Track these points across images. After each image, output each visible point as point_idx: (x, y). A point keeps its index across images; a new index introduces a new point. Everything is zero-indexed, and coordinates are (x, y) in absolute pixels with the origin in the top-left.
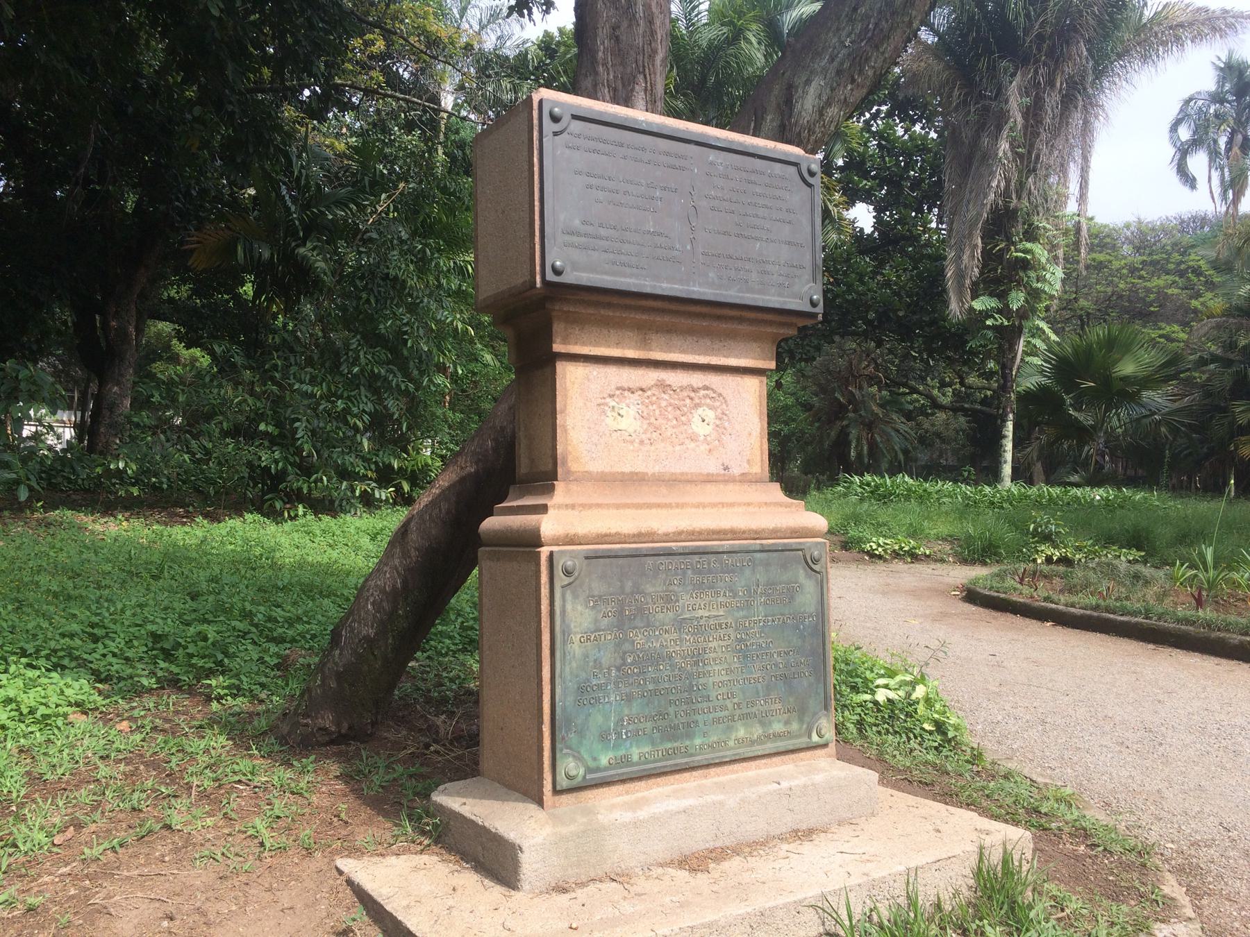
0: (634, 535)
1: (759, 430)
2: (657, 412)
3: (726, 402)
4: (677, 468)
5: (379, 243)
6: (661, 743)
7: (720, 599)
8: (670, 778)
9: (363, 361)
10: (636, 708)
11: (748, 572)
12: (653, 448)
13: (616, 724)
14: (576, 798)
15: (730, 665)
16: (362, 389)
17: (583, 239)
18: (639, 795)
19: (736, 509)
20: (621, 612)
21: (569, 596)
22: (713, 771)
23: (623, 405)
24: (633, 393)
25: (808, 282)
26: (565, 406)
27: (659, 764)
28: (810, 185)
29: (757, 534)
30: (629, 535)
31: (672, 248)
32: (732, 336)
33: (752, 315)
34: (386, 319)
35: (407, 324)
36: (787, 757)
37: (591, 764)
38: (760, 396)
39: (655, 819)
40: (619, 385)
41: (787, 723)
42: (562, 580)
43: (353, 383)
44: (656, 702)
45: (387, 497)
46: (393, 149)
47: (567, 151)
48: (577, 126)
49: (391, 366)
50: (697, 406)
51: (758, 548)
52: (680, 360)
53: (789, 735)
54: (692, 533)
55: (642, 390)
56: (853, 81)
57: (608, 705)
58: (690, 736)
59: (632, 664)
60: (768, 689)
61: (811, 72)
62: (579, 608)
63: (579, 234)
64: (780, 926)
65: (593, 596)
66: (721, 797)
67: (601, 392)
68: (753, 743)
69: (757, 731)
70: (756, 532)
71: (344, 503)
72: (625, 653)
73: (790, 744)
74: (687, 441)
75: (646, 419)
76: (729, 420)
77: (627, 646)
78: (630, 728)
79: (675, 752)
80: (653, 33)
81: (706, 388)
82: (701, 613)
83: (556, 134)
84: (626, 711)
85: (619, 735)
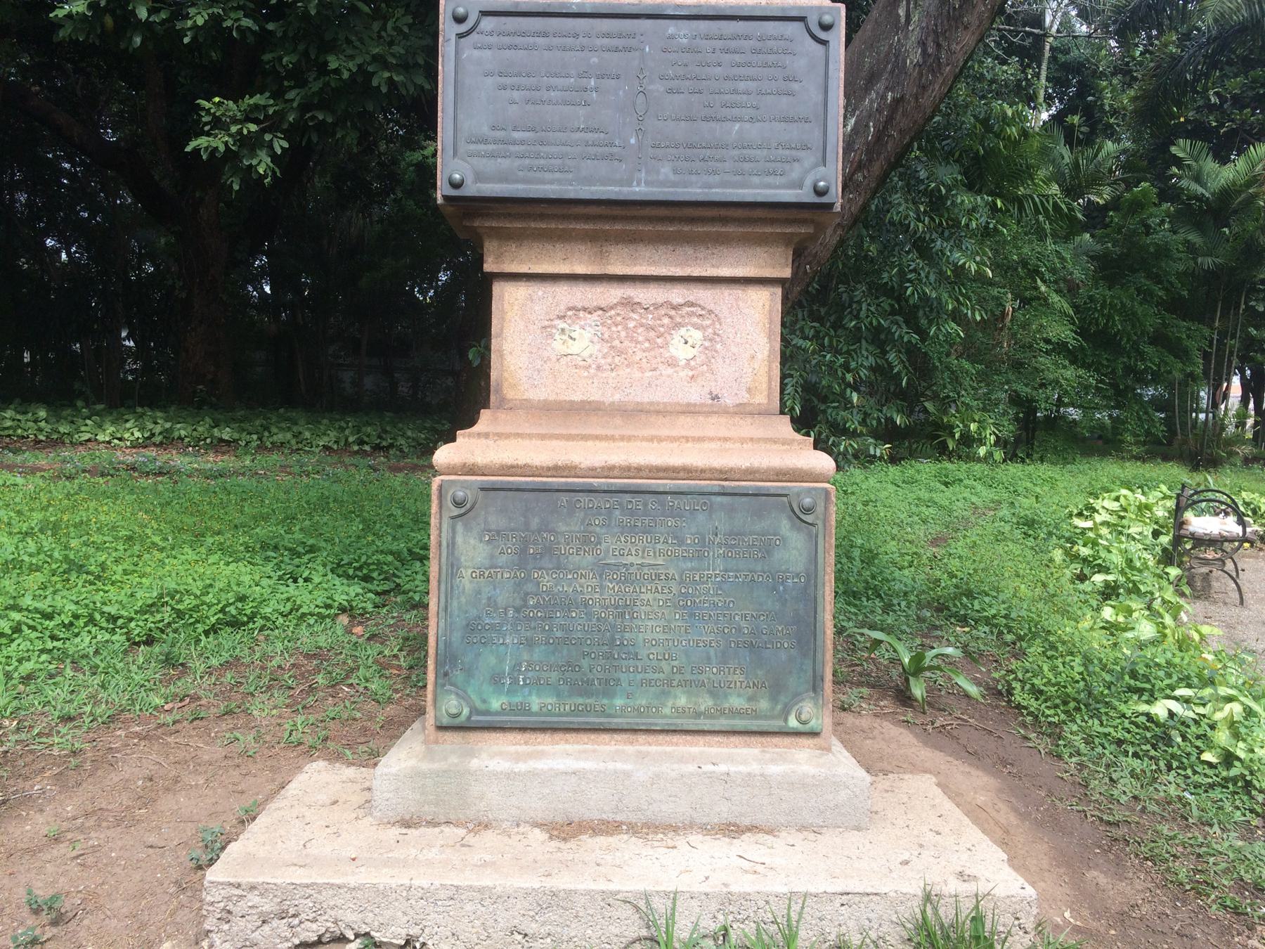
0: (549, 469)
1: (766, 353)
2: (623, 334)
3: (719, 319)
4: (645, 397)
6: (570, 696)
8: (584, 737)
10: (538, 653)
11: (701, 517)
12: (614, 374)
14: (463, 738)
15: (669, 621)
16: (864, 342)
17: (491, 147)
18: (540, 748)
19: (706, 445)
20: (523, 551)
21: (460, 527)
22: (642, 738)
23: (577, 328)
24: (590, 313)
25: (816, 166)
26: (502, 329)
27: (564, 719)
28: (824, 43)
31: (612, 145)
33: (739, 213)
35: (915, 270)
37: (479, 704)
38: (770, 311)
39: (534, 774)
40: (571, 305)
41: (750, 699)
42: (450, 510)
43: (856, 336)
44: (565, 652)
45: (882, 453)
47: (476, 53)
48: (488, 23)
49: (897, 317)
50: (678, 326)
51: (716, 490)
52: (648, 273)
53: (756, 715)
54: (629, 468)
55: (602, 309)
58: (609, 694)
59: (535, 607)
60: (724, 658)
62: (472, 541)
63: (485, 141)
64: (580, 914)
66: (628, 767)
67: (547, 313)
68: (698, 715)
69: (706, 703)
74: (661, 367)
75: (607, 341)
77: (530, 587)
78: (530, 674)
79: (587, 711)
81: (692, 305)
82: (631, 559)
83: (461, 36)
84: (526, 656)
85: (515, 681)
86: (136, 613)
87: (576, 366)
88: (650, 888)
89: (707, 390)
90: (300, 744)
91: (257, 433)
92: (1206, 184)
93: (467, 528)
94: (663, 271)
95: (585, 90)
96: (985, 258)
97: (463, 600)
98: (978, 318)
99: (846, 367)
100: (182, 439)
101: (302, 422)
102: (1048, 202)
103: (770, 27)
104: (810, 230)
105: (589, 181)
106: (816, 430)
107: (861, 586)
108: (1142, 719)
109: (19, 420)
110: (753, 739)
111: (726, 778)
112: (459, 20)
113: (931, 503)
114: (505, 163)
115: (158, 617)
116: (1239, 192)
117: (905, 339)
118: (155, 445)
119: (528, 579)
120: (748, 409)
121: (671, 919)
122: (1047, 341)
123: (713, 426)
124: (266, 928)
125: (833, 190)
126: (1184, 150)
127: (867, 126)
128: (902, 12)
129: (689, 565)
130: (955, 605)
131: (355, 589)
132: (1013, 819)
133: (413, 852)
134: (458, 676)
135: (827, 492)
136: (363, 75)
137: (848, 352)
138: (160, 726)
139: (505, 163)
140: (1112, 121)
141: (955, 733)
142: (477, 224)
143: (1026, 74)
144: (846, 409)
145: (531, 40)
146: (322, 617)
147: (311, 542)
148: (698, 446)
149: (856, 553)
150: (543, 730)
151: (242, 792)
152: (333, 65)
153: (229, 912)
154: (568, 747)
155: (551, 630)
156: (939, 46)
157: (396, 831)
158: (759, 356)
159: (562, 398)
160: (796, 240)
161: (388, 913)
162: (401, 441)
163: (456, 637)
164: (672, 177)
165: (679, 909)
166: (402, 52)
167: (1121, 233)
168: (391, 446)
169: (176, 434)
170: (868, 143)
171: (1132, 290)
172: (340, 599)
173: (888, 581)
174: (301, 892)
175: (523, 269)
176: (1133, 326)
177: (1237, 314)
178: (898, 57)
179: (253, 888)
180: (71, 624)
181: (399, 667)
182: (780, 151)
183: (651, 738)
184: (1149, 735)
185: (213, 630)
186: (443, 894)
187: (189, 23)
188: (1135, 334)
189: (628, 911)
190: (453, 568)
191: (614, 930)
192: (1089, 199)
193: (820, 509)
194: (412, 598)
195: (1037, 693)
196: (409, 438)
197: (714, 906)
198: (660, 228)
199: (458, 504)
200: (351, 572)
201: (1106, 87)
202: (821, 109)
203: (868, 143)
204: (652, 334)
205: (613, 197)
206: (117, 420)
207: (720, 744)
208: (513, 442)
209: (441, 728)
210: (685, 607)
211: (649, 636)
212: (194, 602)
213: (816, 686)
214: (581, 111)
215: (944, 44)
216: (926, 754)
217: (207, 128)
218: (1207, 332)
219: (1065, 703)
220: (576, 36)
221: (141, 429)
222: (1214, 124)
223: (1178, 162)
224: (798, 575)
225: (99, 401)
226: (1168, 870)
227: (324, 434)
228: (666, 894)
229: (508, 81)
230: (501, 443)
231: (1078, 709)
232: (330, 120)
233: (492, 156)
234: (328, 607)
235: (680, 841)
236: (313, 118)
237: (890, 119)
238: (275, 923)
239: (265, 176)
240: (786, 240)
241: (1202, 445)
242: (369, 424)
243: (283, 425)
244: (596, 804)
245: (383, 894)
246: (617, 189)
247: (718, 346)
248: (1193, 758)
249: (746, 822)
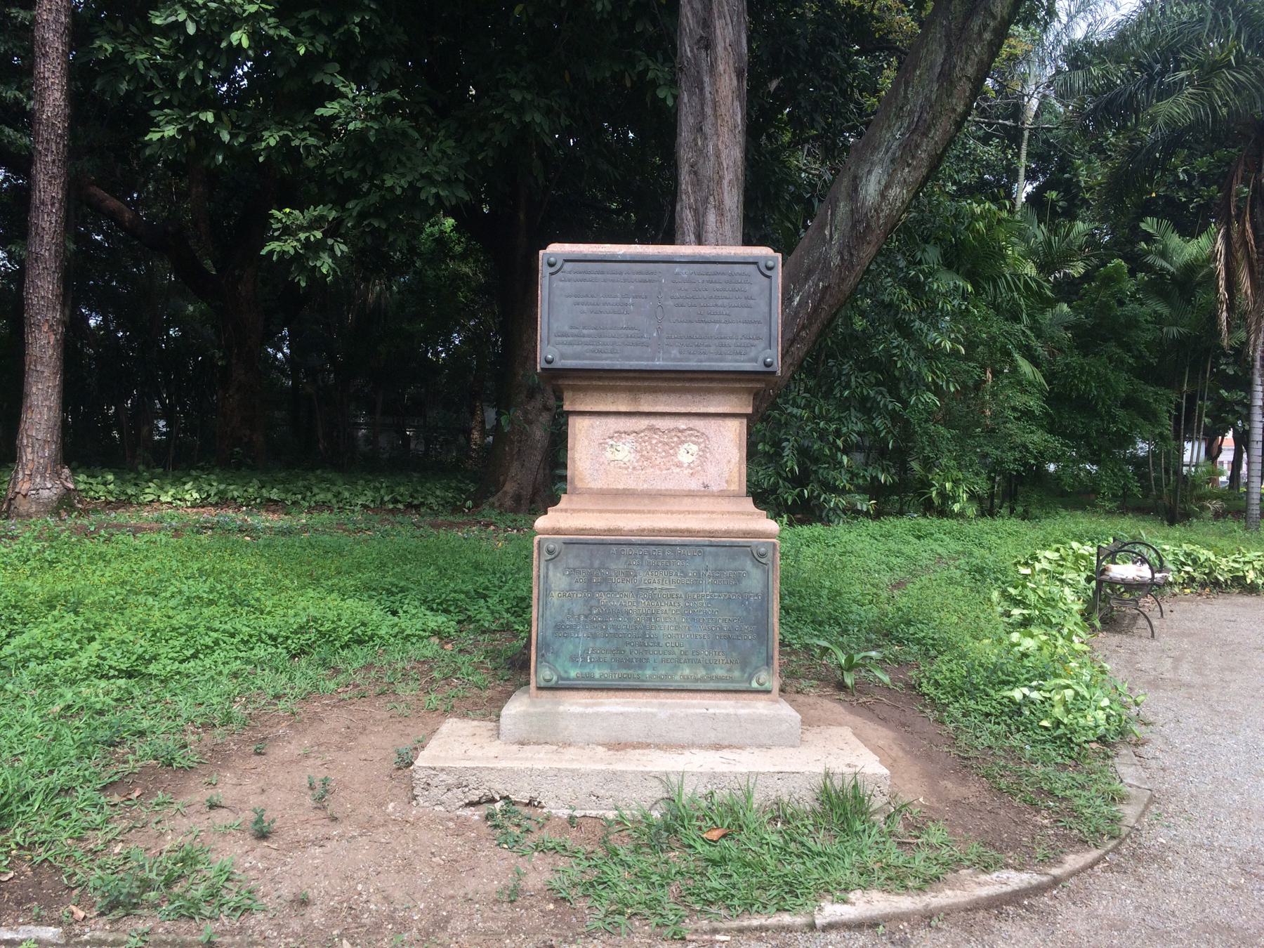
0: (605, 531)
2: (649, 447)
4: (670, 485)
5: (875, 273)
6: (619, 668)
8: (627, 694)
9: (853, 384)
10: (599, 643)
11: (698, 560)
16: (852, 410)
17: (570, 339)
19: (701, 516)
20: (590, 580)
21: (551, 566)
22: (662, 694)
25: (764, 349)
29: (711, 534)
31: (642, 337)
32: (710, 391)
34: (878, 342)
35: (897, 347)
38: (740, 434)
39: (597, 714)
41: (729, 670)
43: (844, 405)
46: (968, 163)
47: (561, 283)
48: (568, 266)
49: (881, 388)
50: (683, 442)
53: (732, 680)
54: (653, 530)
56: (909, 165)
58: (641, 667)
61: (872, 164)
66: (654, 710)
68: (696, 680)
69: (701, 673)
71: (831, 513)
73: (731, 686)
76: (711, 453)
77: (593, 603)
78: (594, 656)
79: (629, 678)
80: (720, 164)
81: (692, 429)
82: (655, 585)
84: (591, 645)
85: (585, 660)
86: (291, 633)
87: (620, 468)
88: (669, 769)
89: (701, 481)
90: (437, 710)
91: (301, 493)
92: (1172, 258)
93: (556, 567)
94: (674, 410)
95: (626, 305)
96: (959, 336)
97: (553, 610)
98: (952, 389)
99: (838, 434)
100: (235, 500)
101: (340, 482)
102: (1019, 280)
103: (737, 268)
104: (763, 385)
105: (628, 358)
106: (809, 488)
107: (824, 617)
108: (1005, 700)
109: (91, 484)
110: (730, 695)
111: (714, 717)
112: (551, 265)
113: (899, 553)
114: (578, 348)
115: (307, 636)
116: (1202, 267)
117: (890, 407)
118: (211, 505)
119: (592, 597)
120: (726, 493)
121: (680, 787)
122: (1014, 409)
123: (705, 504)
124: (449, 793)
125: (775, 363)
126: (1152, 228)
127: (807, 302)
128: (827, 233)
129: (690, 589)
130: (897, 631)
131: (442, 618)
132: (901, 754)
133: (530, 755)
134: (550, 656)
135: (774, 545)
136: (413, 189)
137: (839, 419)
138: (341, 700)
139: (578, 348)
140: (1087, 196)
141: (872, 707)
142: (560, 382)
143: (1006, 154)
144: (835, 469)
145: (594, 276)
146: (421, 638)
147: (402, 584)
148: (695, 516)
149: (825, 592)
150: (601, 689)
151: (409, 735)
152: (389, 183)
153: (429, 784)
154: (617, 700)
155: (606, 628)
156: (852, 255)
157: (516, 747)
158: (733, 461)
159: (611, 487)
160: (755, 391)
161: (519, 784)
162: (431, 500)
163: (549, 633)
164: (678, 356)
165: (685, 781)
166: (446, 170)
167: (1094, 305)
168: (422, 504)
169: (230, 495)
170: (808, 314)
171: (1104, 359)
172: (432, 625)
173: (846, 613)
174: (470, 772)
175: (588, 409)
176: (1107, 393)
177: (1204, 377)
178: (826, 261)
179: (443, 770)
180: (248, 641)
181: (487, 669)
182: (743, 341)
183: (668, 694)
184: (1007, 710)
185: (345, 646)
186: (551, 773)
187: (264, 144)
188: (1109, 399)
189: (656, 783)
190: (547, 592)
191: (649, 794)
192: (1065, 273)
193: (770, 554)
194: (482, 625)
195: (937, 684)
196: (437, 497)
197: (705, 780)
198: (672, 384)
199: (550, 552)
200: (435, 606)
201: (1081, 165)
202: (767, 315)
203: (808, 314)
204: (667, 447)
205: (644, 368)
206: (174, 482)
207: (710, 699)
208: (582, 514)
209: (539, 688)
210: (688, 614)
211: (666, 632)
212: (333, 626)
213: (768, 662)
214: (624, 317)
215: (855, 253)
216: (850, 718)
217: (276, 234)
218: (1173, 397)
219: (954, 690)
220: (621, 273)
221: (199, 491)
222: (1184, 200)
223: (1148, 238)
224: (757, 595)
225: (158, 466)
226: (995, 782)
227: (361, 494)
228: (678, 773)
229: (581, 300)
230: (575, 515)
231: (962, 695)
232: (384, 226)
233: (570, 344)
234: (424, 630)
235: (687, 752)
236: (369, 225)
237: (821, 300)
238: (455, 790)
239: (327, 275)
240: (749, 391)
241: (1175, 500)
242: (399, 484)
243: (323, 485)
244: (635, 731)
245: (515, 773)
246: (645, 363)
247: (708, 455)
248: (1035, 724)
249: (726, 743)
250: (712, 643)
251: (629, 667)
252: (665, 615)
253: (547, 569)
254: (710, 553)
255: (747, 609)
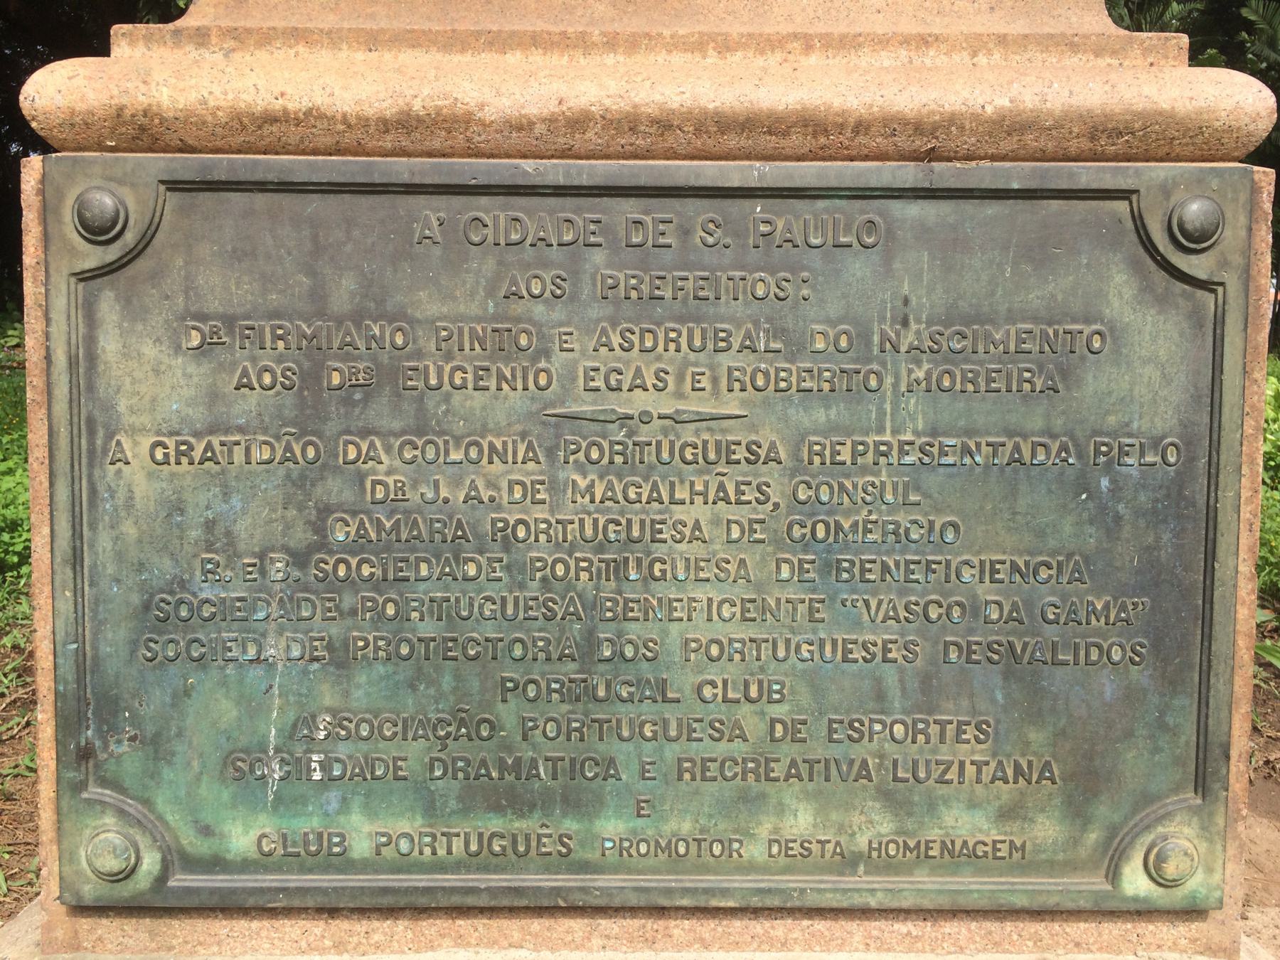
0: (385, 125)
7: (725, 360)
8: (513, 927)
13: (290, 734)
14: (153, 935)
15: (759, 587)
19: (865, 59)
20: (312, 378)
21: (108, 307)
30: (364, 122)
36: (1009, 926)
37: (191, 841)
41: (1007, 814)
42: (73, 252)
44: (447, 682)
57: (257, 672)
65: (203, 317)
68: (849, 862)
70: (919, 127)
72: (325, 511)
77: (335, 489)
78: (343, 750)
82: (641, 401)
85: (297, 769)
93: (132, 309)
155: (402, 616)
210: (806, 544)
211: (701, 631)
224: (1157, 443)
233: (1136, 825)
250: (926, 681)
251: (515, 803)
252: (696, 550)
253: (91, 321)
254: (923, 232)
255: (1110, 523)
